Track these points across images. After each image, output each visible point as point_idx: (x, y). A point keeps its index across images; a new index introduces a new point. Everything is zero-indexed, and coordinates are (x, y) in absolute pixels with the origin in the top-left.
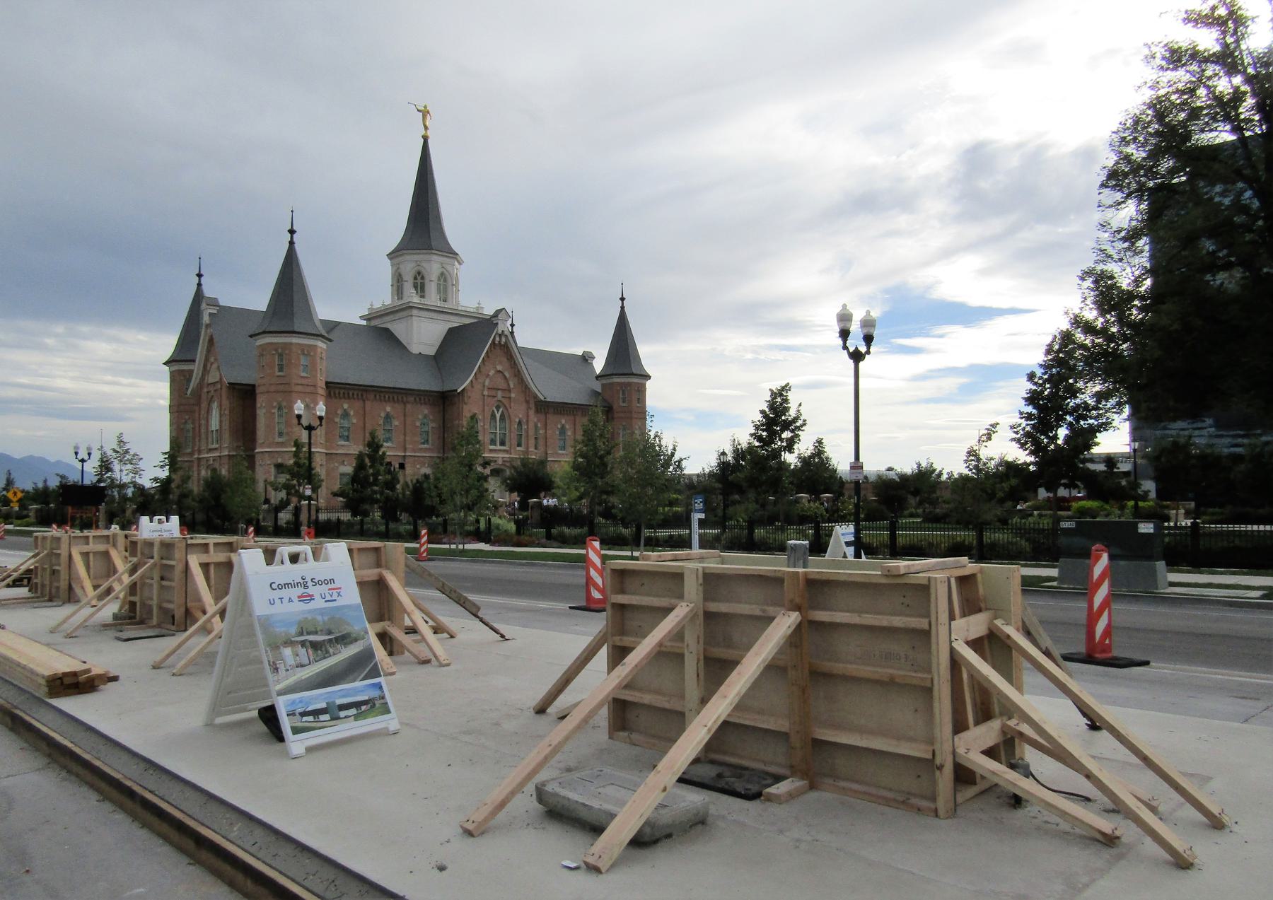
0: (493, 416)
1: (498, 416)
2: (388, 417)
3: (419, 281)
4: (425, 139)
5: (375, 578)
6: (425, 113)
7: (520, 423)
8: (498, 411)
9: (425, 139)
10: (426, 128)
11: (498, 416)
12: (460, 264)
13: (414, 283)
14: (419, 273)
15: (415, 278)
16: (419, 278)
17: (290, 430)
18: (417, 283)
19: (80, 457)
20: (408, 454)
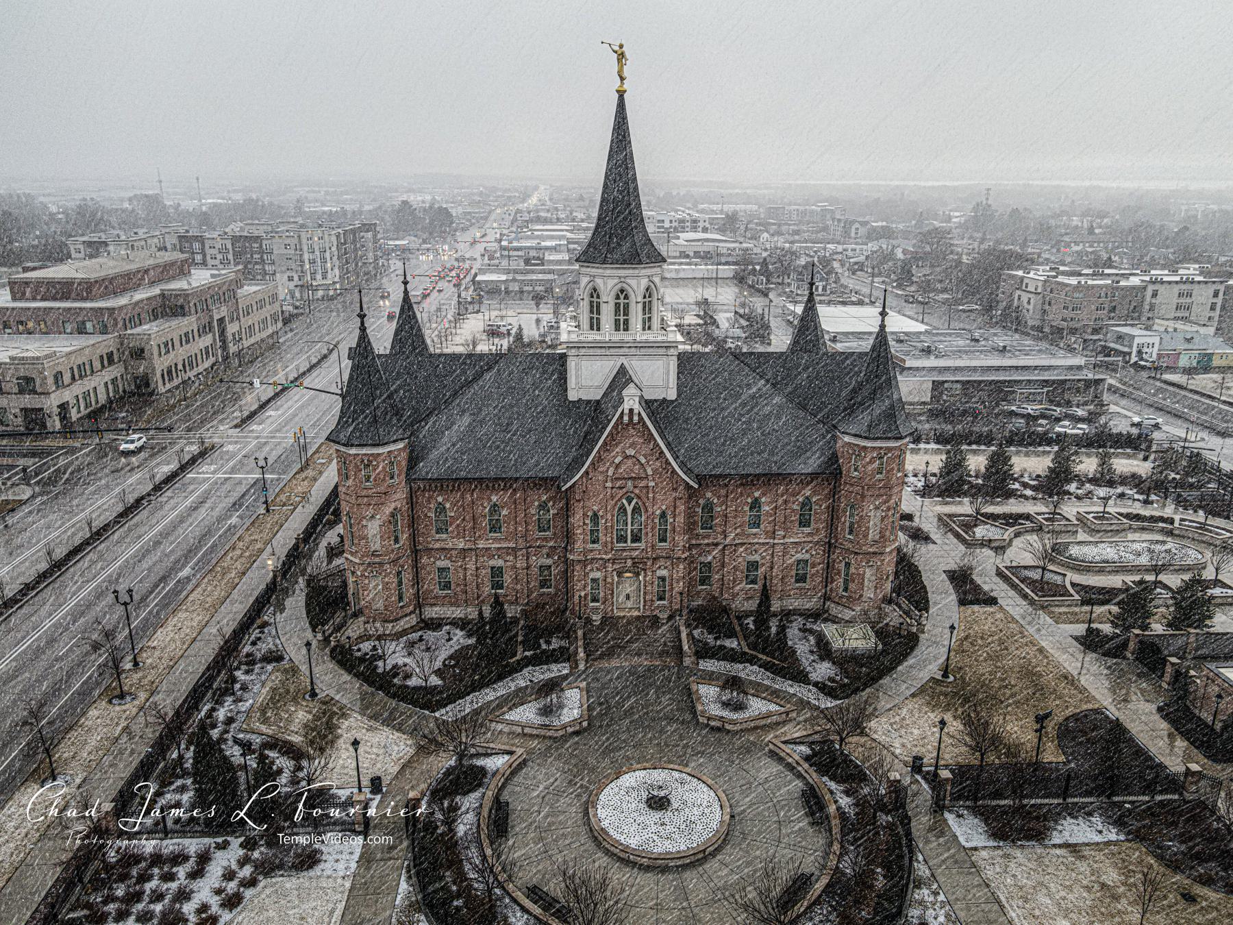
0: (623, 510)
1: (629, 509)
2: (495, 508)
3: (622, 301)
4: (621, 94)
5: (64, 752)
6: (621, 56)
7: (663, 515)
8: (630, 503)
9: (621, 94)
10: (622, 79)
11: (629, 509)
12: (1140, 208)
13: (616, 304)
14: (622, 291)
15: (618, 297)
16: (622, 297)
17: (1152, 457)
18: (619, 304)
19: (260, 465)
20: (776, 541)
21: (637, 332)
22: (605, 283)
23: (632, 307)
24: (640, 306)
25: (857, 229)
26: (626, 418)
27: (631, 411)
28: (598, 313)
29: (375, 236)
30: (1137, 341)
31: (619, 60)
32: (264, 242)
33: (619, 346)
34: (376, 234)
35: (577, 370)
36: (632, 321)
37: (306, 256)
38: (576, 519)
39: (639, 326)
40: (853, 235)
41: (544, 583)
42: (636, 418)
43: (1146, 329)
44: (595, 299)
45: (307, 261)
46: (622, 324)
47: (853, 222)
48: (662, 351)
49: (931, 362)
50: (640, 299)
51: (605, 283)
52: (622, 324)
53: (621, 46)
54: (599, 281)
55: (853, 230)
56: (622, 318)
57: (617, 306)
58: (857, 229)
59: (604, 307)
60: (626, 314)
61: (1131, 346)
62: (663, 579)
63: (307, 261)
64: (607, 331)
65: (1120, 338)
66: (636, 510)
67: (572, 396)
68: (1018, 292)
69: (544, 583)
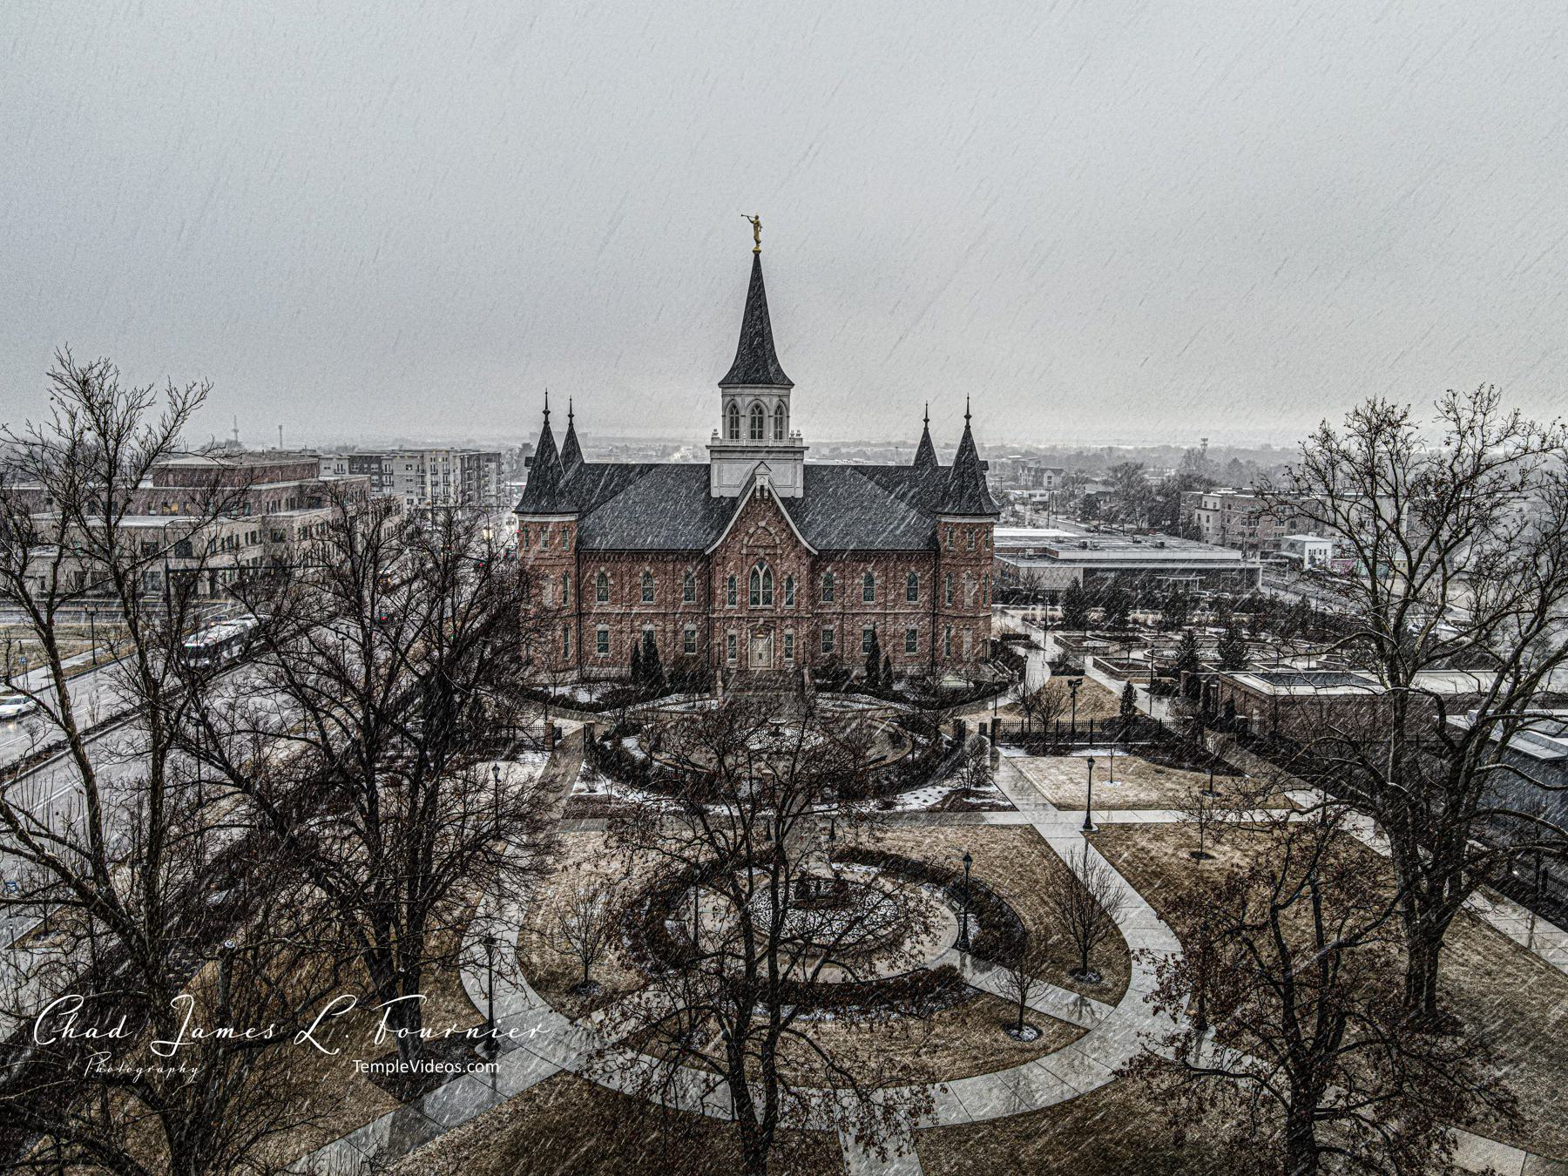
0: (755, 573)
1: (761, 574)
4: (757, 253)
6: (757, 225)
9: (757, 253)
10: (758, 242)
11: (761, 574)
14: (757, 406)
15: (753, 411)
21: (769, 440)
22: (743, 401)
23: (766, 421)
24: (772, 420)
25: (1050, 477)
26: (758, 494)
27: (762, 487)
28: (737, 426)
29: (499, 467)
30: (1308, 547)
31: (755, 228)
32: (384, 463)
33: (757, 450)
34: (499, 466)
35: (719, 472)
36: (765, 433)
37: (428, 478)
38: (717, 583)
39: (772, 434)
40: (1045, 484)
41: (688, 648)
42: (766, 494)
43: (1318, 535)
44: (735, 415)
45: (429, 483)
46: (757, 434)
47: (1043, 471)
48: (790, 456)
49: (1087, 555)
50: (772, 413)
51: (743, 401)
52: (757, 434)
53: (757, 218)
54: (738, 399)
55: (1045, 481)
56: (757, 430)
57: (753, 420)
58: (1050, 477)
59: (742, 420)
60: (761, 426)
61: (1303, 553)
62: (789, 637)
63: (429, 483)
64: (745, 440)
65: (1292, 545)
66: (767, 574)
67: (715, 493)
68: (1197, 511)
69: (688, 648)
